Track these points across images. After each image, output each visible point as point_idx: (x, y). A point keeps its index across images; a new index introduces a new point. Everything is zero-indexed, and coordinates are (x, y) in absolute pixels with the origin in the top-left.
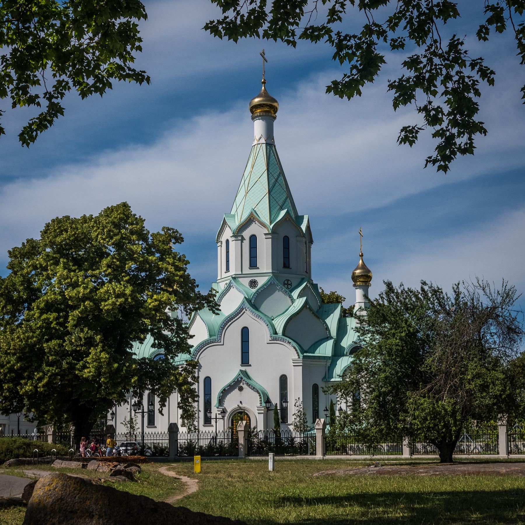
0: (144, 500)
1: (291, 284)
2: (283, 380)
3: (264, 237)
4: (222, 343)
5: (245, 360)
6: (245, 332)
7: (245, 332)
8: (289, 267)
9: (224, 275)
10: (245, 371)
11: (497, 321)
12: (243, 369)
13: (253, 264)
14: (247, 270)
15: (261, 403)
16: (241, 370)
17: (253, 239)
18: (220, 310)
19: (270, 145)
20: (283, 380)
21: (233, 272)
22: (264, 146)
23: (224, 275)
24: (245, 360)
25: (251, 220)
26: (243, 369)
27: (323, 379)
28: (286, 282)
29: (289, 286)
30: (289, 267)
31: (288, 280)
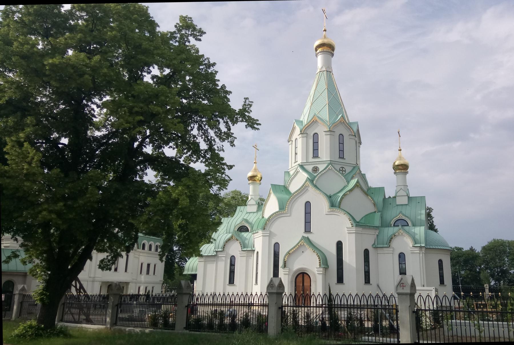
0: (57, 307)
1: (345, 171)
2: (339, 245)
3: (324, 133)
4: (289, 215)
5: (308, 229)
6: (308, 205)
7: (308, 205)
8: (343, 158)
9: (294, 165)
10: (308, 238)
11: (472, 270)
12: (306, 235)
13: (316, 155)
14: (311, 160)
15: (320, 265)
16: (303, 236)
17: (316, 135)
18: (260, 124)
19: (329, 72)
20: (339, 245)
21: (299, 161)
22: (325, 72)
23: (294, 165)
24: (308, 229)
25: (313, 122)
26: (306, 235)
27: (373, 245)
28: (341, 169)
29: (344, 172)
30: (343, 158)
31: (342, 168)
